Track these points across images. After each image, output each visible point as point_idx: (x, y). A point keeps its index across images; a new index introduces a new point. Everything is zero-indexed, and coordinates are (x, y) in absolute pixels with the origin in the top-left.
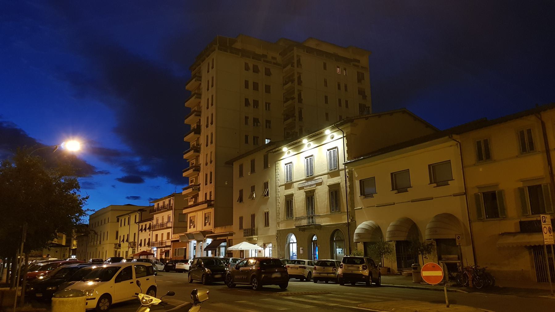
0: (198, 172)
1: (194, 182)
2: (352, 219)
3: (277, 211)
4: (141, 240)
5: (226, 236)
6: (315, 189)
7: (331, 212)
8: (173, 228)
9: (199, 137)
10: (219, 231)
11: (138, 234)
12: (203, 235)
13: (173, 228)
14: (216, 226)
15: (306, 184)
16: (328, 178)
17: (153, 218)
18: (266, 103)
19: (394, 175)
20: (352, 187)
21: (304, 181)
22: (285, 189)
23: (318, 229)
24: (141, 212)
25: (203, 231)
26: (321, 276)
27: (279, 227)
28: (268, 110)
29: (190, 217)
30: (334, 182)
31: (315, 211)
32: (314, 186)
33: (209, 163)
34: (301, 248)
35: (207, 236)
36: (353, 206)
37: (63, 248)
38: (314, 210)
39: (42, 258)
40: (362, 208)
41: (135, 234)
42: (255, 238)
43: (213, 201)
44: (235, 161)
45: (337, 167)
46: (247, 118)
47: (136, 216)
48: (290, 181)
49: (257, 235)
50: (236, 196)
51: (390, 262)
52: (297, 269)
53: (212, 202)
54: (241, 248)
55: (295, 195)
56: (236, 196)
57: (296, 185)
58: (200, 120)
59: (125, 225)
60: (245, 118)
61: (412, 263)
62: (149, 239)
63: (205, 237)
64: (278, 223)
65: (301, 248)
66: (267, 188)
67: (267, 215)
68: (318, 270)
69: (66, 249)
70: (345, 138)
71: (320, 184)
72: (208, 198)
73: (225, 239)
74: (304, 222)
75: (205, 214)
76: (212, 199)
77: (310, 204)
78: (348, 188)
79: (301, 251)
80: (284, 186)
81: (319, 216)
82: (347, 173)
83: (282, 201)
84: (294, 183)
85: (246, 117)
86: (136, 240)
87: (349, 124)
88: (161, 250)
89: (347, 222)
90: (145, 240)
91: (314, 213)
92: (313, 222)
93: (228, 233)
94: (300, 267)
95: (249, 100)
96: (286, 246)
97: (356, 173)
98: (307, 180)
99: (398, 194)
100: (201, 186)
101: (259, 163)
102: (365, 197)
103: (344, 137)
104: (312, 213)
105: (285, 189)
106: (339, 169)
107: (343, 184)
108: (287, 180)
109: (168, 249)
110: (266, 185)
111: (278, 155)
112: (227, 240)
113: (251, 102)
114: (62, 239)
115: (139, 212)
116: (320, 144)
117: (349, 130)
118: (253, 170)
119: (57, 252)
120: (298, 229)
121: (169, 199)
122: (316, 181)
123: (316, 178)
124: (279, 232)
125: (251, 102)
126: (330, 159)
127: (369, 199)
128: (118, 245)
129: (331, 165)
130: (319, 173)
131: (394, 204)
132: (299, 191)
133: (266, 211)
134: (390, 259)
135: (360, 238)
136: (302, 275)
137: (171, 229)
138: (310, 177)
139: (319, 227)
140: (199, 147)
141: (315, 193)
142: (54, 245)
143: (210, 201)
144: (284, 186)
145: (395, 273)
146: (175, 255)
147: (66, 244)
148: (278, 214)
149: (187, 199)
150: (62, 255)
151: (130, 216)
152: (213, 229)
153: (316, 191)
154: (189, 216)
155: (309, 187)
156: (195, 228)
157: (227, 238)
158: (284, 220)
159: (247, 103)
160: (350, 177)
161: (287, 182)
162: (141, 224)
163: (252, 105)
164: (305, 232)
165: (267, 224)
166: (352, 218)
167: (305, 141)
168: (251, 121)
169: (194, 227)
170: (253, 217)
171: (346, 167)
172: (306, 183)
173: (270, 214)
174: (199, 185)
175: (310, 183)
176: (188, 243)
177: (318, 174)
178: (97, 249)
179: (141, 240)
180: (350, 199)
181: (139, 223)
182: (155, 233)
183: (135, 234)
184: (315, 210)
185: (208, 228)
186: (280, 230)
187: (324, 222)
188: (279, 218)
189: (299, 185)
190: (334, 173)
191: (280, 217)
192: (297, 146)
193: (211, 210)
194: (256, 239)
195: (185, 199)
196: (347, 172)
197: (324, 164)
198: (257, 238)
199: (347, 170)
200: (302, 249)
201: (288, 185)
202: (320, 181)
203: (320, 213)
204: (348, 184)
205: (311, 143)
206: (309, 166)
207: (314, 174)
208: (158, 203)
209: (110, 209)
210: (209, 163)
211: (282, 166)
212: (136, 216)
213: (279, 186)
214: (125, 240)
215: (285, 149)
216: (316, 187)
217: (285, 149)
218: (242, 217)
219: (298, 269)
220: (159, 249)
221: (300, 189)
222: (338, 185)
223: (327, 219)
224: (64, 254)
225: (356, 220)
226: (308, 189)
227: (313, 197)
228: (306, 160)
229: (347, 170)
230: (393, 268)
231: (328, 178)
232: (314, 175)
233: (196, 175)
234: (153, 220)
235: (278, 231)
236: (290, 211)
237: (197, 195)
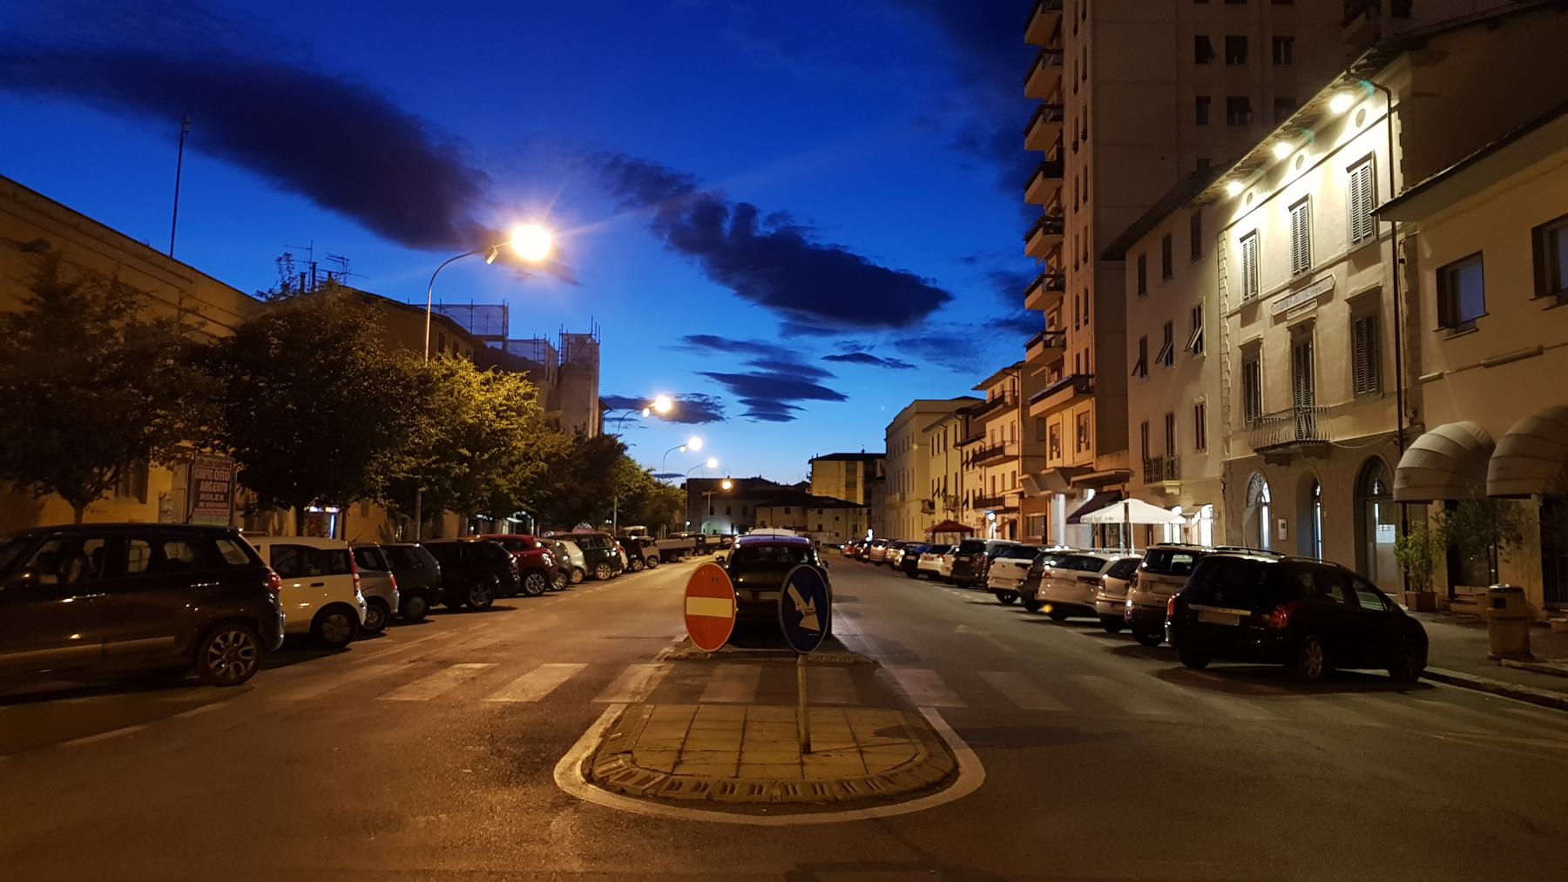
0: (1058, 294)
1: (1056, 323)
2: (1412, 416)
3: (1224, 400)
4: (968, 492)
5: (1118, 483)
6: (1314, 318)
7: (1356, 396)
8: (1020, 459)
9: (1058, 186)
10: (1106, 466)
11: (962, 476)
12: (1064, 478)
13: (1020, 459)
14: (1100, 452)
15: (1293, 302)
16: (1350, 273)
17: (985, 432)
18: (1276, 41)
19: (1546, 236)
20: (1414, 298)
21: (1287, 293)
22: (1243, 325)
23: (1320, 457)
24: (965, 415)
25: (1075, 465)
26: (1116, 613)
27: (1228, 451)
28: (1283, 62)
29: (1051, 427)
30: (1365, 284)
31: (1313, 392)
32: (1312, 307)
33: (1081, 262)
34: (1280, 522)
35: (1074, 482)
36: (1416, 369)
37: (852, 509)
38: (1311, 390)
39: (805, 533)
40: (1441, 376)
41: (956, 474)
42: (1170, 486)
43: (1092, 376)
44: (1129, 247)
45: (1373, 228)
46: (1202, 102)
47: (956, 426)
48: (1252, 296)
49: (1179, 479)
50: (1133, 358)
51: (1523, 577)
52: (1071, 583)
53: (1091, 382)
54: (1111, 519)
55: (1265, 344)
56: (1133, 358)
57: (1268, 309)
58: (1061, 131)
59: (938, 452)
60: (1197, 103)
61: (1493, 580)
62: (981, 490)
63: (1069, 484)
64: (1226, 441)
65: (1280, 522)
66: (1200, 325)
67: (1200, 410)
68: (1110, 592)
69: (861, 514)
70: (1395, 116)
71: (1325, 298)
72: (1083, 372)
73: (1119, 492)
74: (1288, 433)
75: (1079, 416)
76: (1090, 373)
77: (1303, 375)
78: (1404, 305)
79: (1282, 531)
80: (1239, 315)
81: (1325, 412)
82: (1402, 246)
83: (1234, 363)
84: (1263, 303)
85: (1198, 99)
86: (959, 493)
87: (1405, 59)
88: (1003, 518)
89: (1397, 429)
90: (974, 492)
91: (1312, 402)
92: (1308, 435)
93: (1113, 472)
94: (1081, 579)
95: (1212, 44)
96: (1250, 511)
97: (1425, 245)
98: (1296, 286)
99: (1560, 308)
100: (1068, 333)
101: (1181, 248)
102: (1457, 332)
103: (1391, 110)
104: (1307, 402)
105: (1243, 325)
106: (1378, 236)
107: (1388, 292)
108: (1246, 294)
109: (1013, 516)
110: (1197, 316)
111: (1218, 214)
112: (1123, 493)
113: (1218, 46)
114: (856, 487)
115: (960, 417)
116: (1328, 149)
117: (1406, 81)
118: (1167, 272)
119: (837, 519)
120: (1264, 457)
121: (1011, 377)
122: (1317, 286)
123: (1318, 278)
124: (1229, 465)
125: (1218, 46)
126: (1355, 203)
127: (1466, 341)
128: (927, 503)
129: (1355, 224)
130: (1325, 258)
131: (1540, 351)
132: (1275, 327)
133: (1197, 400)
134: (1525, 568)
135: (1410, 487)
136: (1084, 604)
137: (1017, 462)
138: (1302, 278)
139: (1325, 450)
140: (1061, 216)
141: (1316, 331)
142: (831, 502)
143: (1087, 376)
144: (1239, 315)
145: (1539, 620)
146: (1028, 534)
147: (864, 502)
148: (1226, 409)
149: (1041, 372)
150: (850, 528)
151: (946, 427)
152: (1094, 461)
153: (1319, 324)
154: (1050, 421)
155: (1299, 313)
156: (1060, 459)
157: (1123, 487)
158: (1242, 430)
159: (1203, 50)
160: (1408, 263)
161: (1245, 300)
162: (965, 449)
163: (1223, 55)
164: (1291, 469)
165: (1201, 444)
166: (1414, 412)
167: (1281, 149)
168: (1217, 110)
169: (1059, 456)
170: (1170, 419)
171: (1397, 223)
172: (1293, 298)
173: (1207, 412)
174: (1063, 332)
175: (1303, 296)
176: (1050, 501)
177: (1322, 262)
178: (899, 512)
179: (968, 492)
180: (1411, 339)
181: (962, 445)
182: (991, 471)
183: (956, 474)
184: (1314, 389)
185: (1087, 457)
186: (1230, 461)
187: (1334, 431)
188: (1229, 423)
189: (1275, 305)
190: (1361, 256)
191: (1230, 420)
192: (1268, 172)
193: (1087, 405)
194: (1176, 492)
195: (1033, 375)
196: (1400, 243)
197: (1337, 225)
198: (1180, 487)
199: (1400, 237)
200: (1283, 526)
201: (1248, 312)
202: (1325, 287)
203: (1327, 402)
204: (1403, 289)
205: (1305, 152)
206: (1299, 236)
207: (1312, 265)
208: (992, 388)
209: (914, 410)
210: (1081, 262)
211: (1232, 250)
212: (956, 426)
213: (1228, 317)
214: (941, 490)
215: (1233, 187)
216: (1319, 309)
217: (1233, 187)
218: (1146, 424)
219: (1074, 586)
220: (999, 516)
221: (1278, 319)
222: (1374, 293)
223: (1344, 421)
224: (856, 525)
225: (1426, 423)
226: (1296, 317)
227: (1308, 344)
228: (1290, 215)
229: (1400, 237)
230: (1532, 602)
231: (1350, 273)
232: (1312, 267)
233: (1055, 302)
234: (984, 436)
235: (1225, 463)
236: (1253, 397)
237: (1061, 361)
